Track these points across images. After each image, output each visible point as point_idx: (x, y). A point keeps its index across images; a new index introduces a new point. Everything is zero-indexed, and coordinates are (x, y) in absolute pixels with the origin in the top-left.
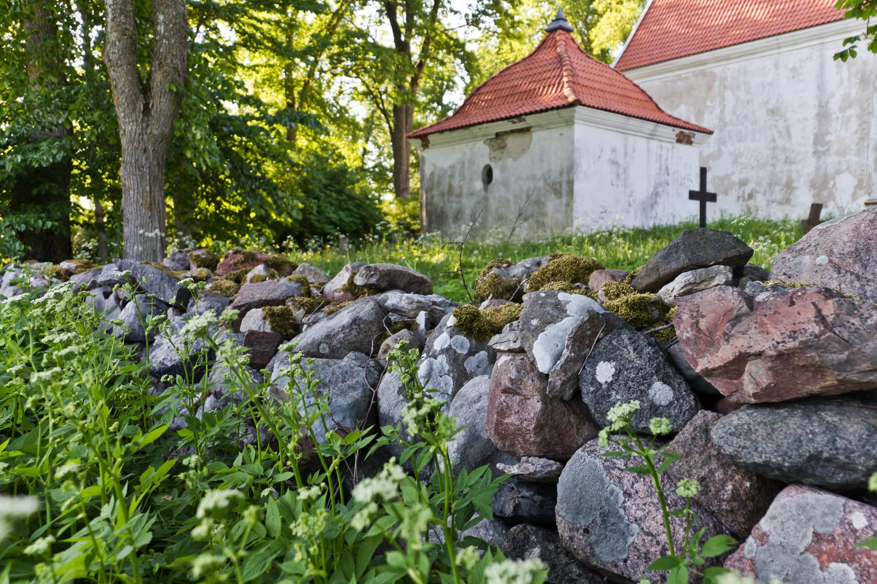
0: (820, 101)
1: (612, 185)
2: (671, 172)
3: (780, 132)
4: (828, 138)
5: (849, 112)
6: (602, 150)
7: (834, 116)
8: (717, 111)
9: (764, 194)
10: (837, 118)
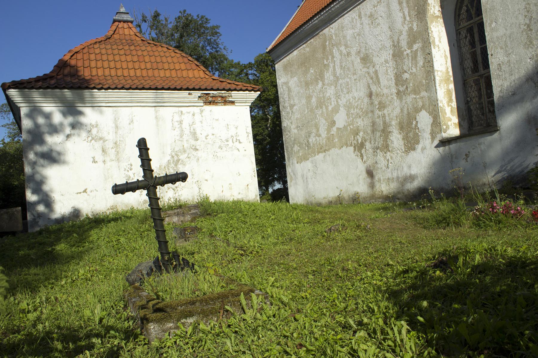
0: (393, 42)
1: (95, 162)
2: (201, 137)
3: (372, 78)
4: (406, 76)
5: (416, 47)
6: (117, 127)
7: (405, 53)
8: (331, 69)
9: (370, 143)
10: (408, 54)
